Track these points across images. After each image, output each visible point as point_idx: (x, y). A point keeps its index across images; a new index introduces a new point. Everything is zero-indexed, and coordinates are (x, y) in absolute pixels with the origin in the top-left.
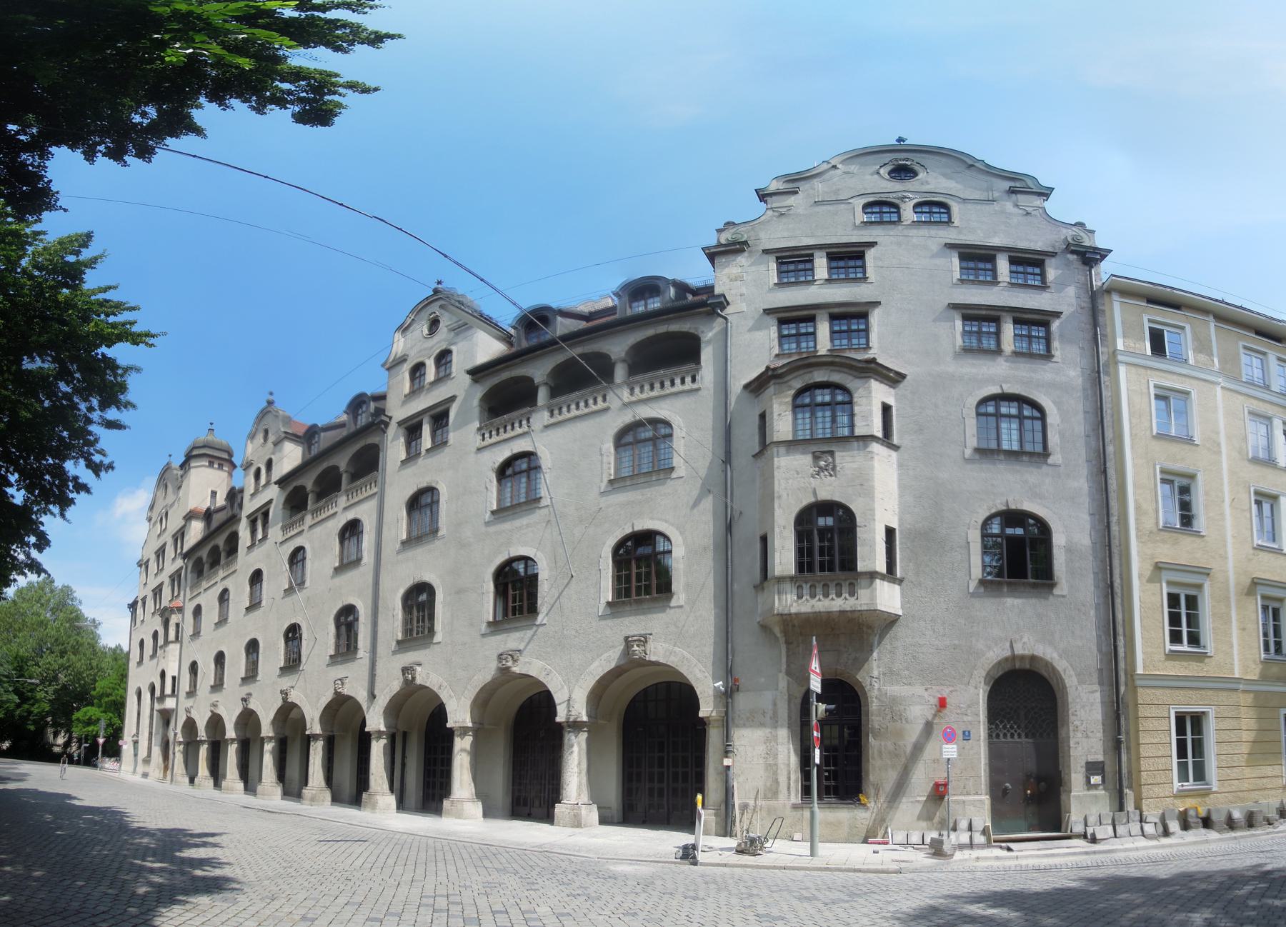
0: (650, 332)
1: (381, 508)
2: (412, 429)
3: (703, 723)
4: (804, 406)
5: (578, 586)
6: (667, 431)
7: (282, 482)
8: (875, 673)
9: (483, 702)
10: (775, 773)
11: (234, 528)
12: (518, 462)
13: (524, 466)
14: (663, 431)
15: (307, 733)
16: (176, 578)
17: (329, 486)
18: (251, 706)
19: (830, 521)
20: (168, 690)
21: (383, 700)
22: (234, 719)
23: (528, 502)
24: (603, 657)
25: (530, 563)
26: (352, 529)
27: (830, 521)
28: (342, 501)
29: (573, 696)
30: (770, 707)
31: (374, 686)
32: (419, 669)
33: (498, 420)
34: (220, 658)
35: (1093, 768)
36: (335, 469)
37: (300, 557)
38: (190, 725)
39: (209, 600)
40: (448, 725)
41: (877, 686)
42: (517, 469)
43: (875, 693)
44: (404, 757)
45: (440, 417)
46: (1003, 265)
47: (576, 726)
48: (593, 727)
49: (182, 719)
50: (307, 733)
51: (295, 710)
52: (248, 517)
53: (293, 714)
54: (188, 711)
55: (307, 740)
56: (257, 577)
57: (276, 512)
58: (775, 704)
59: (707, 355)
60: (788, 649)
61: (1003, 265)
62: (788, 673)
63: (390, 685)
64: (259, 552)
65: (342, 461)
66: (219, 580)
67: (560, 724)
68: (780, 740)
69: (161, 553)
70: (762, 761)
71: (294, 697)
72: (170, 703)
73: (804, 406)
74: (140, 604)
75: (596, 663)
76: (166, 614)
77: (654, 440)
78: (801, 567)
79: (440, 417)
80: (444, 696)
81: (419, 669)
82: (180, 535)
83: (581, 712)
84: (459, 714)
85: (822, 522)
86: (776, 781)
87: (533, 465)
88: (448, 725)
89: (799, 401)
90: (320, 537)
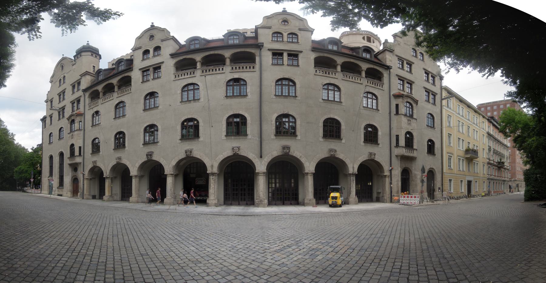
0: (181, 58)
1: (134, 97)
2: (145, 71)
4: (230, 85)
6: (198, 87)
9: (143, 167)
14: (196, 87)
19: (238, 120)
20: (77, 153)
21: (267, 159)
23: (194, 100)
27: (238, 120)
28: (115, 95)
33: (205, 68)
35: (439, 188)
45: (157, 68)
46: (285, 55)
47: (213, 174)
48: (176, 176)
59: (257, 59)
61: (285, 55)
72: (78, 160)
73: (230, 85)
77: (194, 89)
79: (157, 68)
83: (215, 170)
84: (134, 171)
85: (235, 120)
89: (229, 84)
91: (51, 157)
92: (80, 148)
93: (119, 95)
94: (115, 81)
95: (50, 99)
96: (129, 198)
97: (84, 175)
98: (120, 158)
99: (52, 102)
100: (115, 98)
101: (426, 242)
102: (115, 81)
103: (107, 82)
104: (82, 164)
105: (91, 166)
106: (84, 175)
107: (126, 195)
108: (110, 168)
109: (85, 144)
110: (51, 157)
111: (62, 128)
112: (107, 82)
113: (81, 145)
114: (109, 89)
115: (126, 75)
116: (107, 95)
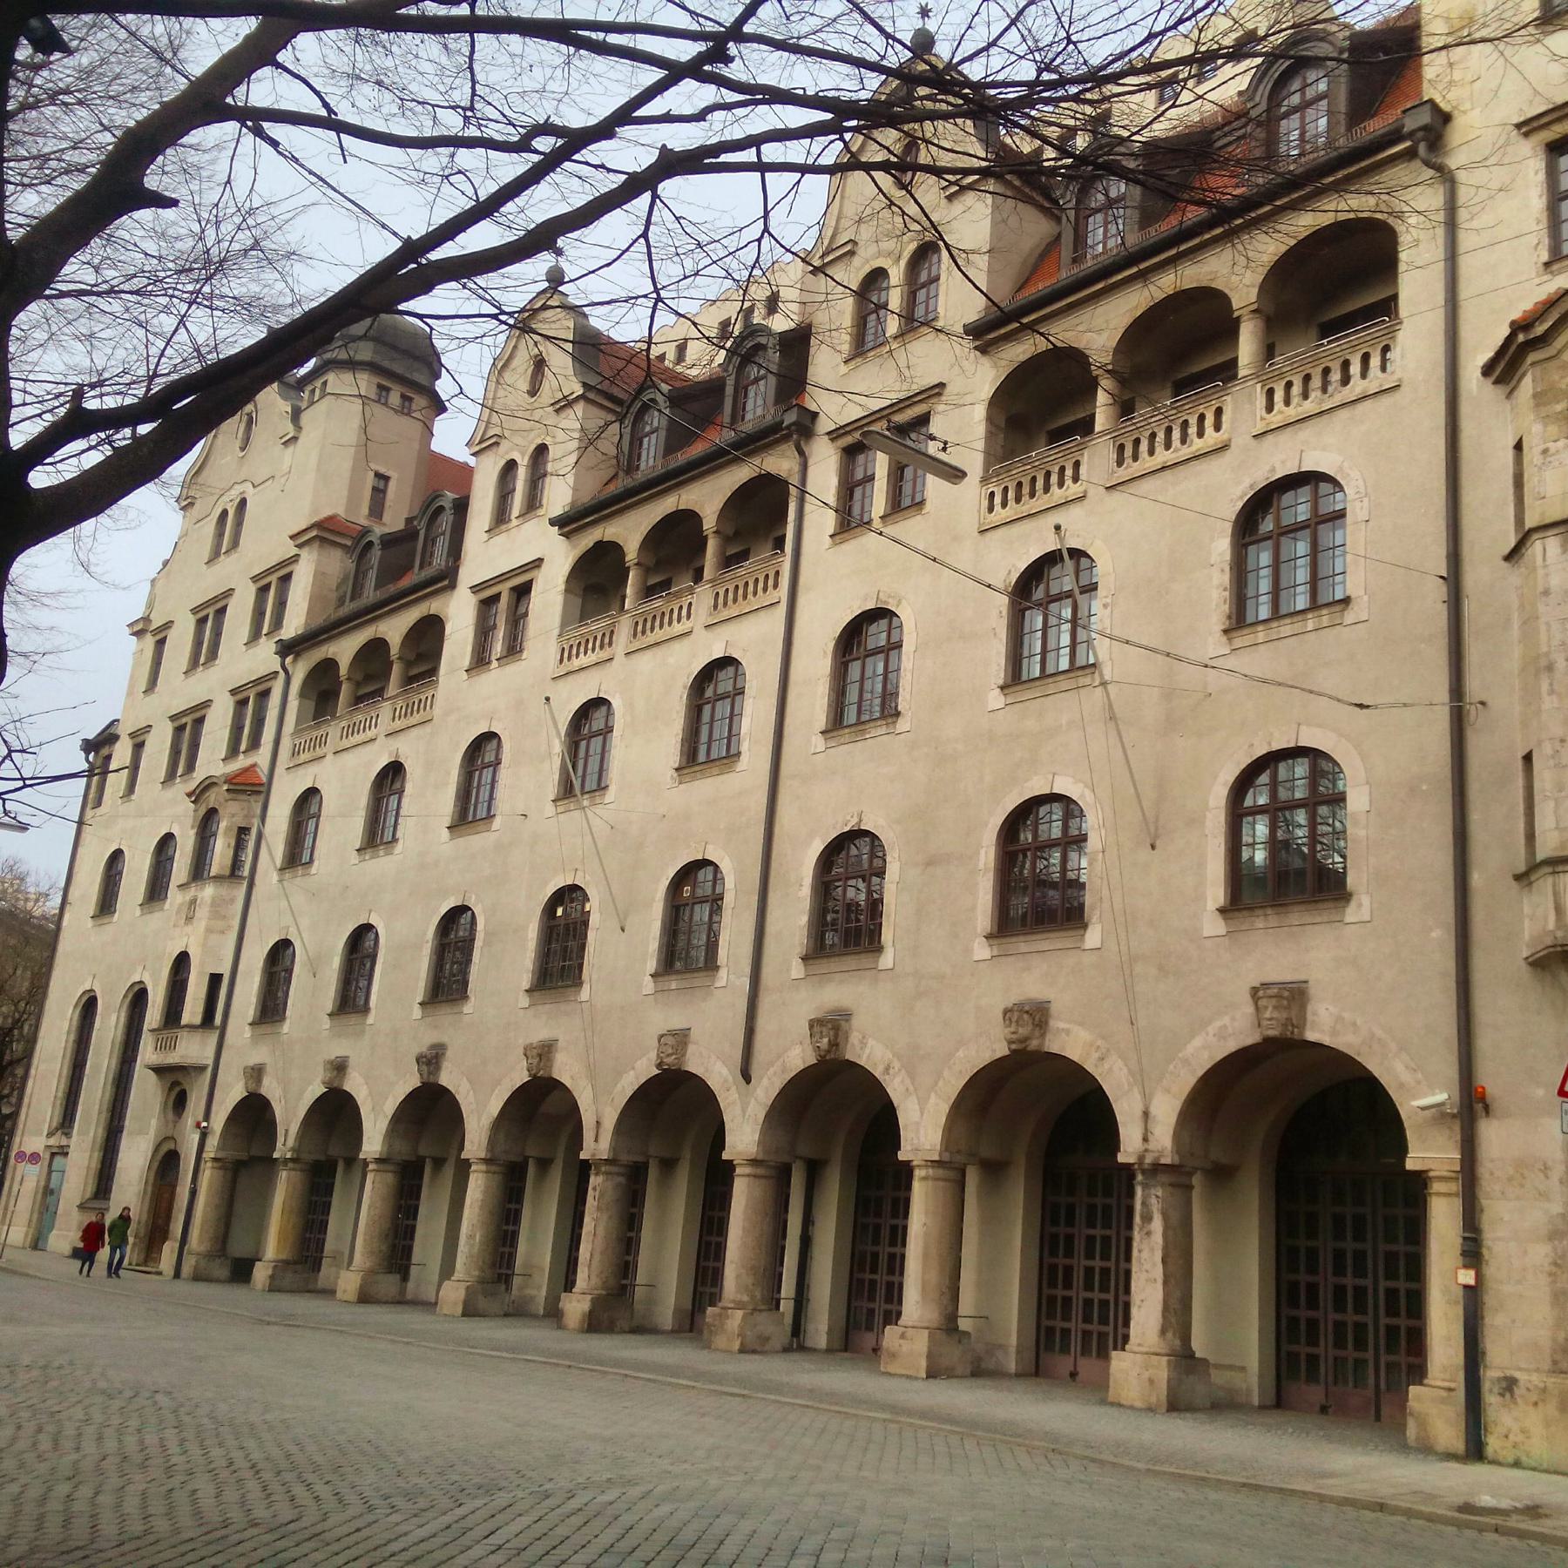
3: (1419, 1183)
5: (1159, 877)
11: (434, 606)
12: (1287, 498)
13: (1303, 512)
16: (251, 700)
18: (445, 1079)
20: (192, 1010)
21: (768, 1086)
22: (391, 1106)
24: (1211, 1029)
28: (1242, 407)
29: (1153, 1110)
31: (745, 1042)
34: (361, 944)
37: (597, 722)
38: (254, 1114)
39: (344, 777)
40: (902, 1156)
42: (1287, 519)
44: (808, 1221)
49: (232, 1093)
51: (555, 1095)
52: (475, 589)
53: (551, 1105)
54: (256, 1073)
56: (482, 753)
57: (549, 598)
63: (788, 1053)
64: (498, 677)
67: (1128, 1166)
69: (211, 615)
70: (1544, 1280)
71: (566, 1070)
72: (193, 1049)
75: (1197, 1042)
76: (212, 798)
80: (896, 1089)
82: (273, 584)
87: (1326, 507)
88: (902, 1156)
90: (646, 681)
91: (89, 1006)
92: (215, 980)
93: (1282, 413)
94: (1238, 270)
95: (156, 624)
96: (1103, 1355)
97: (204, 1135)
98: (1036, 1014)
99: (161, 643)
100: (1248, 436)
101: (179, 1426)
102: (1238, 270)
103: (1166, 283)
104: (210, 1069)
105: (799, 1056)
106: (204, 1135)
107: (1072, 1320)
108: (1185, 1080)
109: (241, 967)
110: (89, 1006)
111: (490, 736)
112: (1166, 283)
113: (225, 969)
114: (1182, 354)
115: (1354, 204)
116: (1298, 352)
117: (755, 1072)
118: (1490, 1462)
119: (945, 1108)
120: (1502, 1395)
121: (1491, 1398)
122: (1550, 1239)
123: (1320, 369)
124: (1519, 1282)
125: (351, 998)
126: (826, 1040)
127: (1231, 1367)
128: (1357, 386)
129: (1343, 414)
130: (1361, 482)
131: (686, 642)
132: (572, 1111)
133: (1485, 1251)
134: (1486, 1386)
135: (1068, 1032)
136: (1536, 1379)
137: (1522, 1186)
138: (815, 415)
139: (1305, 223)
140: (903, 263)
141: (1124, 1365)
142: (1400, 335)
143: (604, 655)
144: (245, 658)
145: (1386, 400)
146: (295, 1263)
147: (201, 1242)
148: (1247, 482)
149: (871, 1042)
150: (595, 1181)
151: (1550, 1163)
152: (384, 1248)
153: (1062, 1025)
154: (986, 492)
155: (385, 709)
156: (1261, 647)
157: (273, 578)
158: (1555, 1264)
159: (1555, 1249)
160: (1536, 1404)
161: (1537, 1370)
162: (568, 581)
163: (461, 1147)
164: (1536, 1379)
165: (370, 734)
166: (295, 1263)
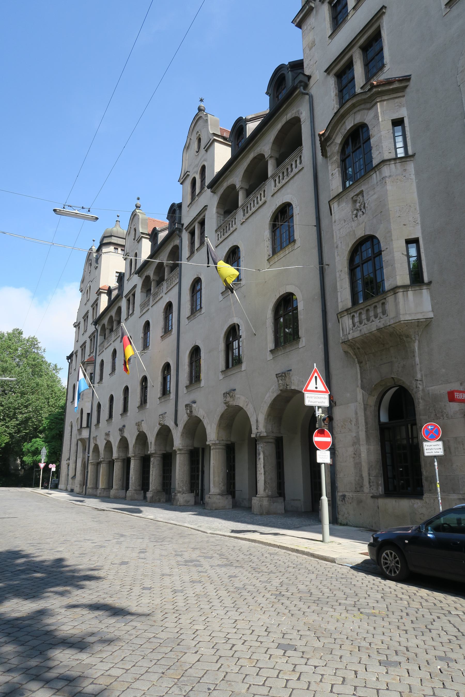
7: (214, 185)
8: (419, 376)
10: (360, 470)
15: (253, 436)
17: (257, 177)
25: (375, 241)
26: (283, 213)
28: (270, 187)
30: (354, 416)
32: (194, 405)
36: (261, 158)
41: (421, 387)
43: (420, 394)
50: (253, 436)
55: (254, 443)
58: (356, 414)
60: (360, 367)
62: (363, 387)
65: (266, 147)
66: (169, 295)
68: (361, 443)
70: (352, 460)
71: (240, 401)
74: (74, 356)
75: (268, 395)
78: (355, 301)
81: (194, 405)
86: (361, 476)
90: (253, 230)
103: (251, 156)
117: (178, 423)
118: (341, 524)
119: (215, 426)
120: (342, 501)
121: (339, 502)
122: (353, 445)
123: (286, 169)
124: (346, 461)
125: (233, 361)
126: (189, 411)
127: (297, 500)
128: (295, 170)
129: (291, 181)
130: (296, 202)
131: (162, 300)
132: (246, 419)
133: (336, 452)
134: (338, 498)
135: (239, 398)
136: (350, 494)
137: (345, 428)
138: (309, 77)
139: (279, 126)
140: (198, 174)
141: (255, 501)
142: (303, 151)
143: (147, 308)
144: (91, 329)
145: (301, 173)
146: (107, 489)
147: (90, 485)
148: (271, 212)
149: (200, 410)
150: (260, 447)
151: (352, 419)
152: (120, 483)
153: (238, 396)
154: (217, 235)
155: (240, 212)
156: (277, 263)
157: (95, 305)
158: (355, 454)
159: (354, 449)
160: (351, 503)
161: (352, 491)
162: (141, 289)
163: (173, 445)
164: (350, 494)
165: (161, 296)
166: (107, 489)
